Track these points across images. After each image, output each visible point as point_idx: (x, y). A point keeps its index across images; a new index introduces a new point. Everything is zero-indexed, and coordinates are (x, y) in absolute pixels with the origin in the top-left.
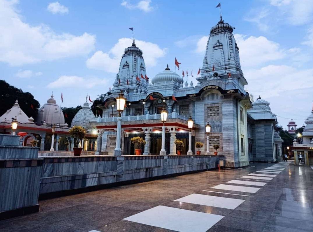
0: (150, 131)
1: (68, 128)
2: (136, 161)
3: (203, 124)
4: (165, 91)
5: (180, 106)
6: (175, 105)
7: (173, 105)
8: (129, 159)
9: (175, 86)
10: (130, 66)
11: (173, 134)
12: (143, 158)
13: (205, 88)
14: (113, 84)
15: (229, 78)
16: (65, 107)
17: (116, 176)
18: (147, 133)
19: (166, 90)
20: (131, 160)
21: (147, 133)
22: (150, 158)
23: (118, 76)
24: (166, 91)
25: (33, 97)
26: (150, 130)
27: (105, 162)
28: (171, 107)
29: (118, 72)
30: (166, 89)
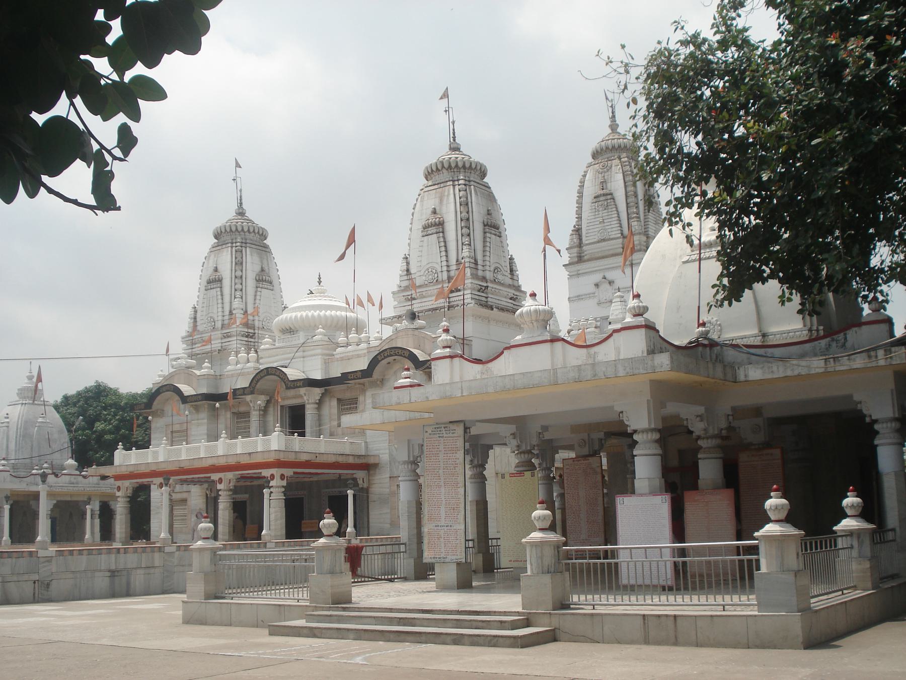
0: (230, 483)
1: (78, 473)
2: (84, 558)
3: (385, 454)
4: (302, 359)
5: (339, 400)
6: (327, 399)
7: (319, 400)
8: (66, 553)
9: (475, 286)
10: (224, 281)
11: (885, 425)
12: (137, 550)
13: (382, 354)
14: (183, 338)
15: (442, 322)
16: (86, 388)
17: (37, 582)
18: (644, 431)
19: (303, 357)
20: (70, 555)
21: (224, 490)
22: (122, 551)
23: (196, 312)
24: (304, 361)
25: (169, 54)
26: (230, 480)
27: (14, 560)
28: (316, 406)
29: (194, 301)
30: (306, 354)
